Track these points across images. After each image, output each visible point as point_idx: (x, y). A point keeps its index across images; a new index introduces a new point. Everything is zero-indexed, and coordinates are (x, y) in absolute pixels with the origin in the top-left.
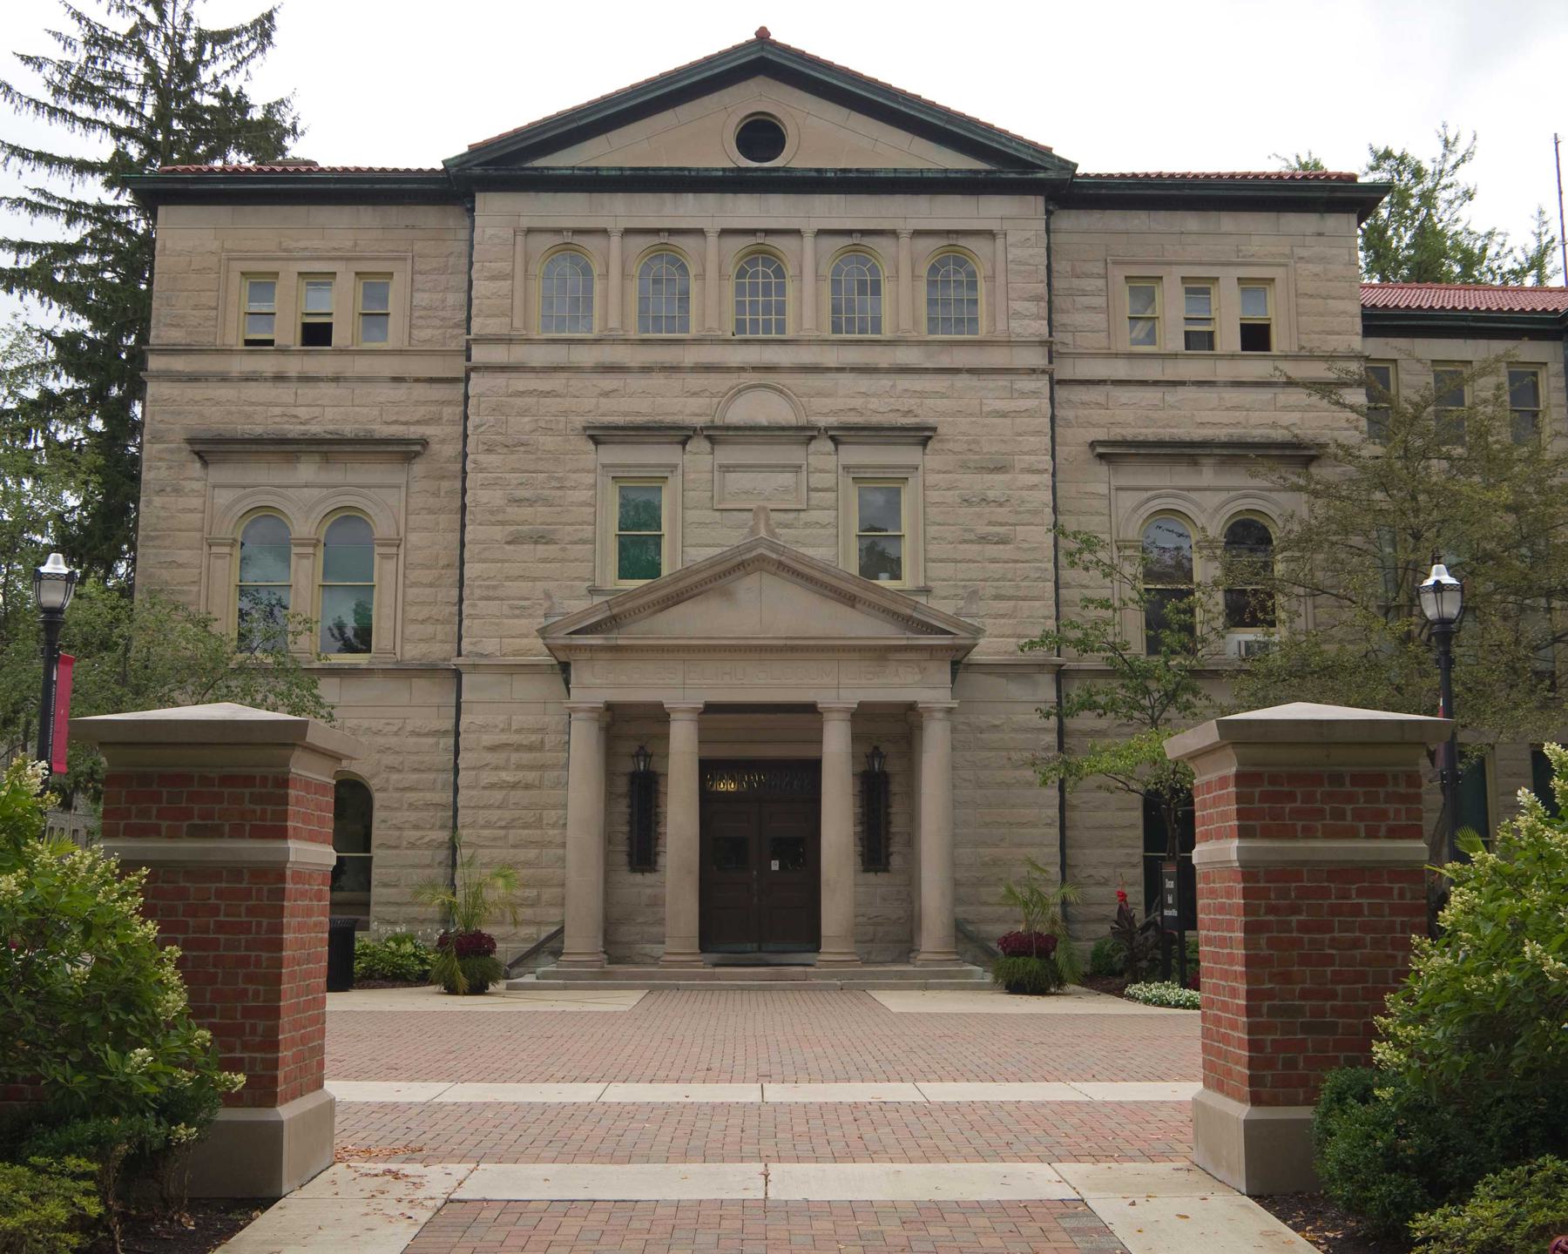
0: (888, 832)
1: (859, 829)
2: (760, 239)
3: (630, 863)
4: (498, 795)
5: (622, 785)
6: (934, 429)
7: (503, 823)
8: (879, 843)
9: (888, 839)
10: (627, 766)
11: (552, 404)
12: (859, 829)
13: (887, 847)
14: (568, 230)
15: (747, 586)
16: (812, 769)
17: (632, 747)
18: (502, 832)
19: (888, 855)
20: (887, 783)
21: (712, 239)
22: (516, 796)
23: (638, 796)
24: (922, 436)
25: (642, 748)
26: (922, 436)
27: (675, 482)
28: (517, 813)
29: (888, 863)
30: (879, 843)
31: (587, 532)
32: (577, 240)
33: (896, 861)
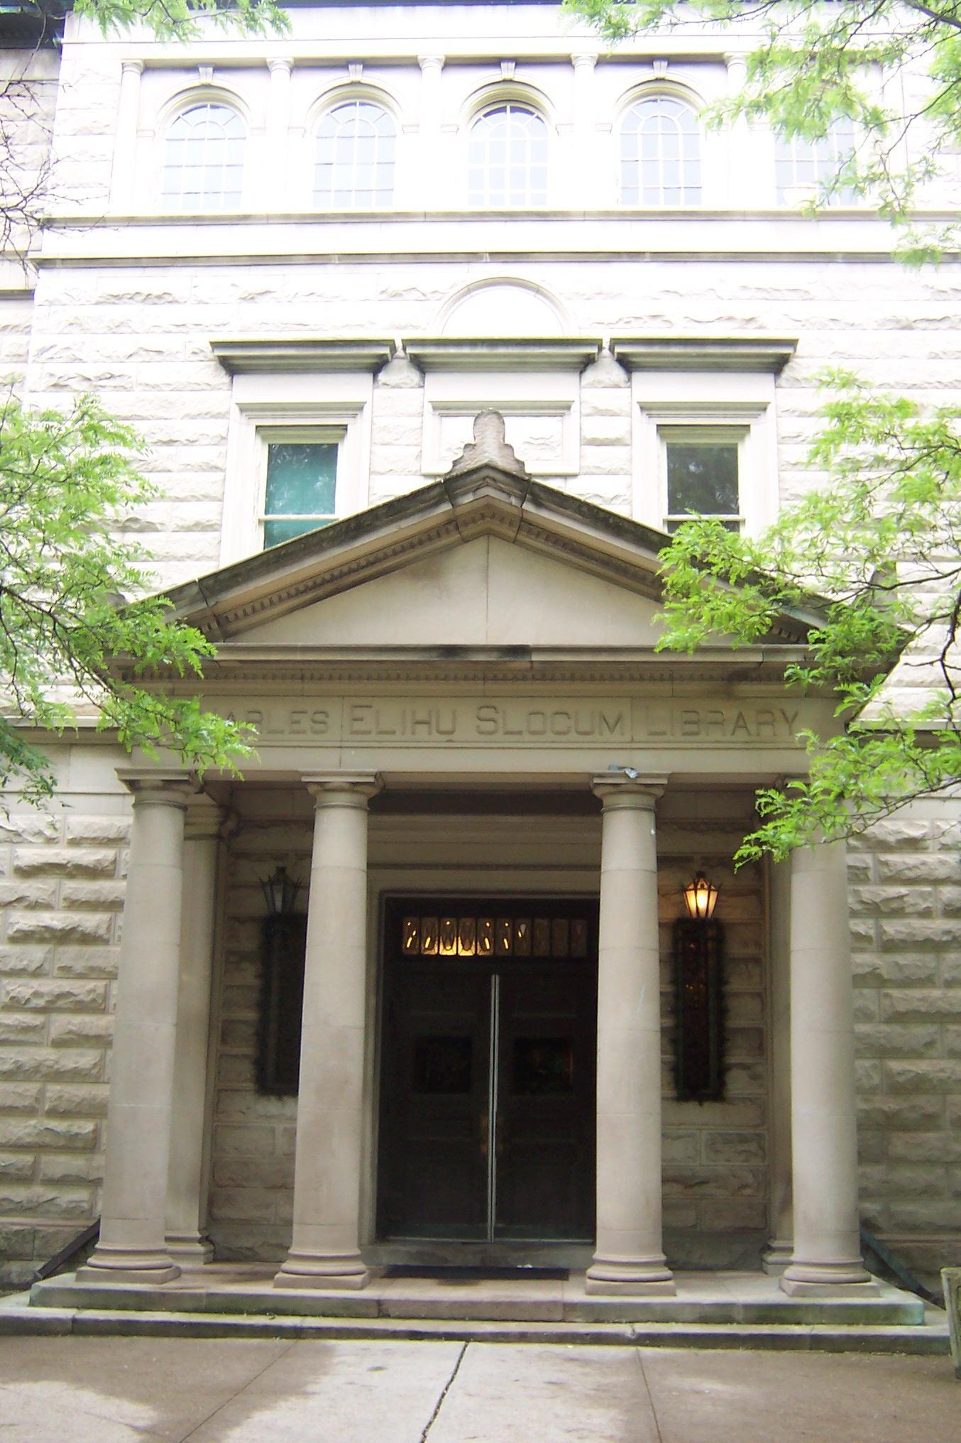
0: (721, 1028)
1: (669, 1057)
2: (508, 71)
3: (289, 1101)
4: (36, 954)
5: (249, 940)
6: (792, 343)
7: (41, 1002)
8: (713, 1040)
9: (722, 1040)
10: (256, 904)
11: (167, 315)
12: (669, 1022)
13: (721, 1054)
14: (206, 64)
15: (467, 565)
16: (585, 911)
17: (267, 870)
18: (37, 1020)
19: (722, 1071)
20: (720, 940)
21: (432, 69)
22: (70, 954)
23: (257, 943)
24: (774, 360)
25: (281, 870)
26: (774, 360)
27: (358, 431)
28: (66, 985)
29: (722, 1084)
30: (713, 1040)
31: (205, 512)
32: (221, 80)
33: (737, 1083)
